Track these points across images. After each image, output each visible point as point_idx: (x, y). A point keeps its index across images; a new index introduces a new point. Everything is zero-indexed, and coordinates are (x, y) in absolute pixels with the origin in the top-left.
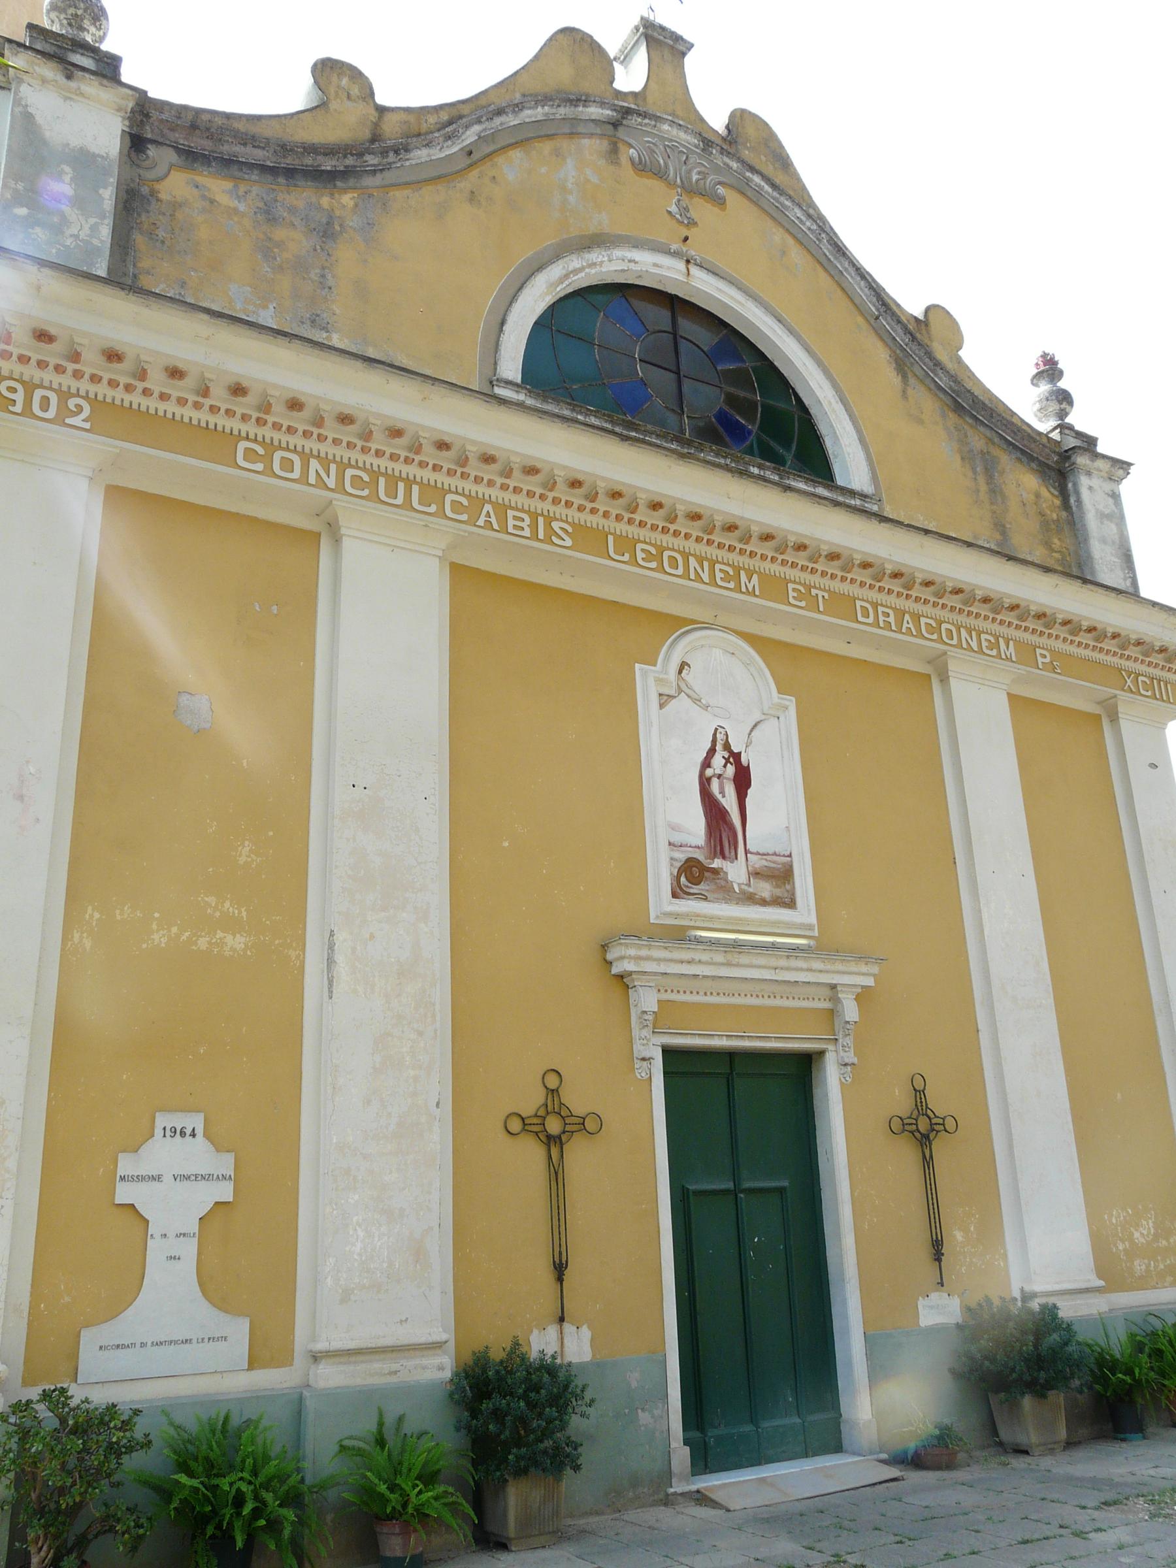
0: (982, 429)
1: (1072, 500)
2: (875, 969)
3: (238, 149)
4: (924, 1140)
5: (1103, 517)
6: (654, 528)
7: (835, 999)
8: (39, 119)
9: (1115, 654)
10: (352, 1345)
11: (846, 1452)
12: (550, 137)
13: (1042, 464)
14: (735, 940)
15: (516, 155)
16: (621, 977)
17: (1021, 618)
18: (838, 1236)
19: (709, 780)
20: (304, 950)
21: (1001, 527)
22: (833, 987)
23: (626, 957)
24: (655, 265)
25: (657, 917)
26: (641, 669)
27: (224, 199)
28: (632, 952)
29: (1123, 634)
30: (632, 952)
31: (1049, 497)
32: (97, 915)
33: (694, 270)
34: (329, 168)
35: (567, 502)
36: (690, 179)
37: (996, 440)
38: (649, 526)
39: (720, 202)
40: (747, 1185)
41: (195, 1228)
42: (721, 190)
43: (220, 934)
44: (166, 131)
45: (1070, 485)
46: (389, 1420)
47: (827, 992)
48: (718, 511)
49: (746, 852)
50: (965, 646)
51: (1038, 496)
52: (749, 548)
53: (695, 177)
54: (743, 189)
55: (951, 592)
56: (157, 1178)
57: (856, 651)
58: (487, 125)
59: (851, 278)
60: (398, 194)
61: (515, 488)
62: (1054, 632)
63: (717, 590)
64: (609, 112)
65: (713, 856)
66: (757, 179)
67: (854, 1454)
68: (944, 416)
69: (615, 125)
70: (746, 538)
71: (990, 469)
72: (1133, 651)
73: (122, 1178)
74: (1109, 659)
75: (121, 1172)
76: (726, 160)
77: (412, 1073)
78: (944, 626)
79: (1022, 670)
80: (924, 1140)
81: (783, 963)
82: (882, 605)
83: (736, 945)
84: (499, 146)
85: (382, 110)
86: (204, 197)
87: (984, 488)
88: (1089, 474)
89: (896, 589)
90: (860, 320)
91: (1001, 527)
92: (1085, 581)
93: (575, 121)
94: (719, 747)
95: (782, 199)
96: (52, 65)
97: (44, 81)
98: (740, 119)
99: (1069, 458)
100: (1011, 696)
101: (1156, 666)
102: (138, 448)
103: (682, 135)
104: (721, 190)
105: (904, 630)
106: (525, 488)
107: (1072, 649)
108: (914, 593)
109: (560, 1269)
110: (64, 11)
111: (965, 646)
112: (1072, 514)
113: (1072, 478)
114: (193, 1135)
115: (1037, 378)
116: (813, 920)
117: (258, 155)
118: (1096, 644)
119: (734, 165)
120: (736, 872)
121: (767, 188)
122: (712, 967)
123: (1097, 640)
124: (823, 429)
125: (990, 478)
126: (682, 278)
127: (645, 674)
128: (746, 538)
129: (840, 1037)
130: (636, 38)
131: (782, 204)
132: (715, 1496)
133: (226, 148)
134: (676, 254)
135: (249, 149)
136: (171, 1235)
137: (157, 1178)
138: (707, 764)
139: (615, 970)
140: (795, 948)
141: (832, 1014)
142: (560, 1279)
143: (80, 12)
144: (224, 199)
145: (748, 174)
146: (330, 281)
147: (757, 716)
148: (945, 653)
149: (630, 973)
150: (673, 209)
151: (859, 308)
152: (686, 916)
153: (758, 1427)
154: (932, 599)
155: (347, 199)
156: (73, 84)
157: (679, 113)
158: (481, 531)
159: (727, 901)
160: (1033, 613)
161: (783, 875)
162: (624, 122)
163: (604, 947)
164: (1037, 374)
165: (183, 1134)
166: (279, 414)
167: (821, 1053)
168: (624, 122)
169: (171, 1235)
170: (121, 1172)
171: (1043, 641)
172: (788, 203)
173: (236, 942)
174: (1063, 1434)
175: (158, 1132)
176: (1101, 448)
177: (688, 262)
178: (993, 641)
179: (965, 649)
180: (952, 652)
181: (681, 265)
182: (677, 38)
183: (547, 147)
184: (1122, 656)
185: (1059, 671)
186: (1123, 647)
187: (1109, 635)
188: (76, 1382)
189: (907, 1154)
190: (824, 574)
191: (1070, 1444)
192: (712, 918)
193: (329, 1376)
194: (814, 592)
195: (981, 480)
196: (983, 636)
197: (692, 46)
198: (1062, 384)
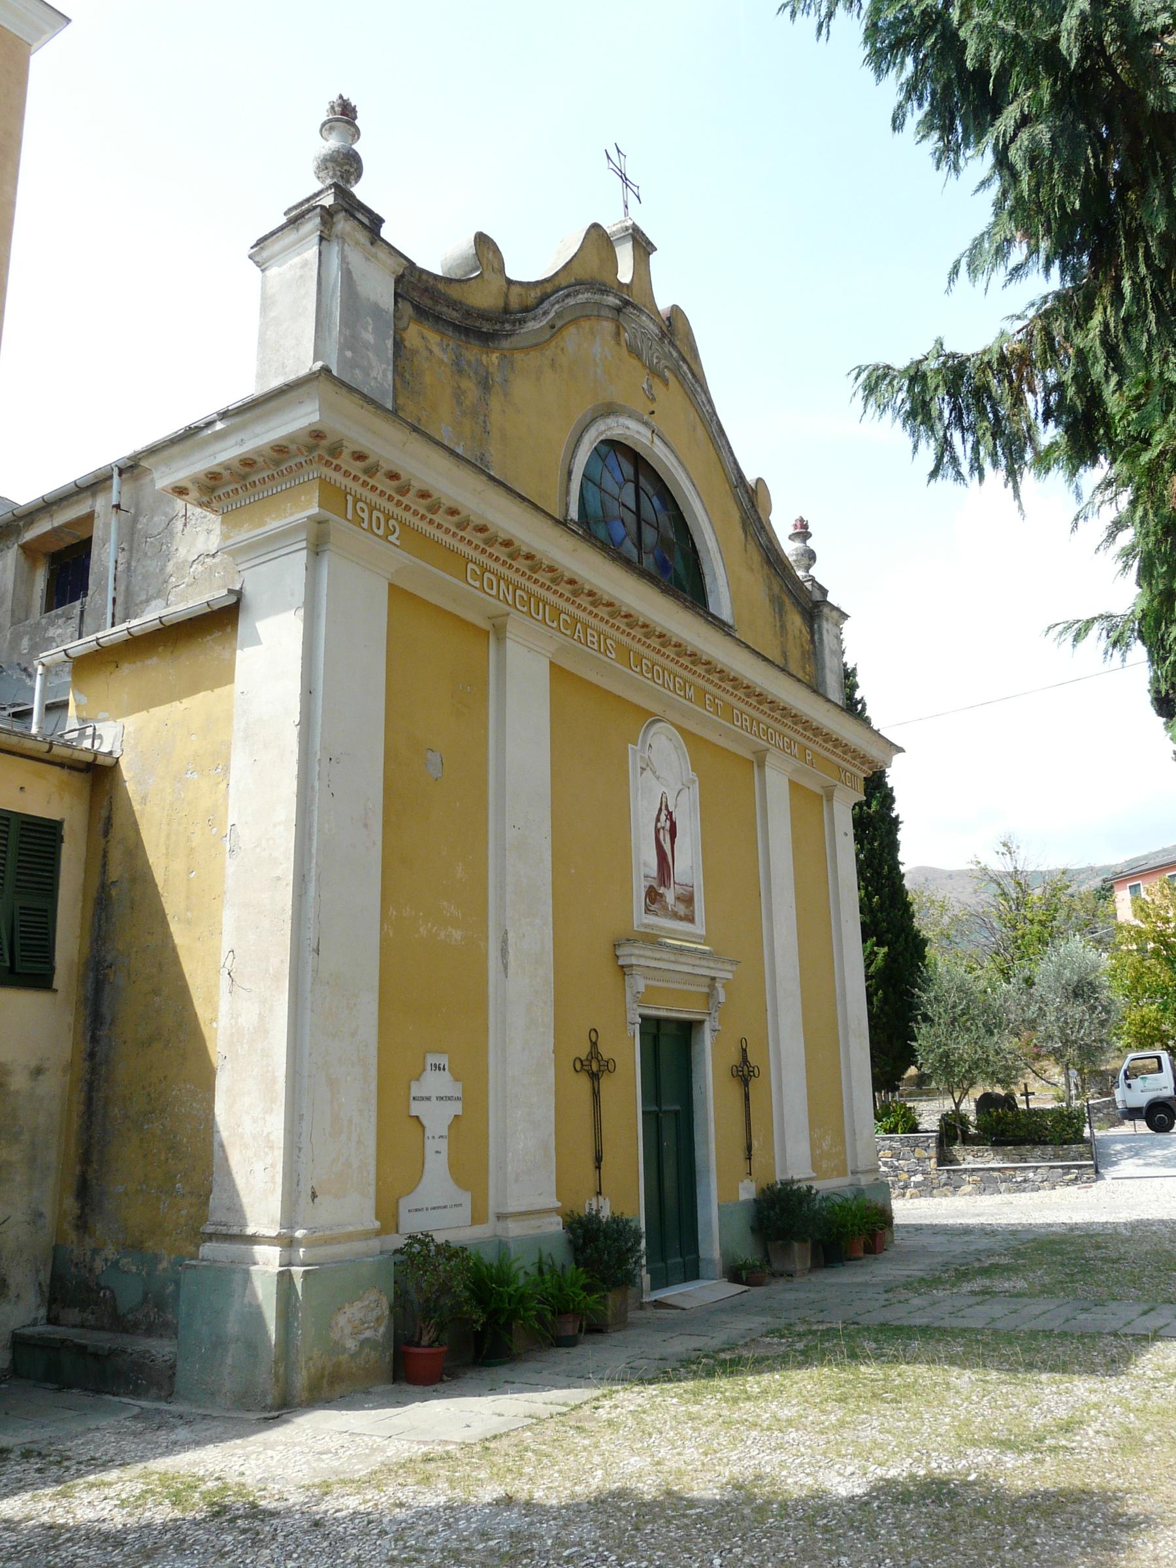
0: (778, 578)
1: (816, 637)
2: (734, 968)
3: (445, 309)
4: (594, 1077)
5: (833, 652)
6: (416, 513)
7: (712, 987)
8: (355, 277)
9: (523, 574)
10: (523, 1209)
11: (703, 1279)
12: (588, 317)
13: (804, 608)
14: (681, 946)
15: (572, 330)
16: (622, 967)
17: (612, 615)
18: (706, 1142)
19: (659, 830)
20: (487, 942)
21: (784, 655)
22: (713, 979)
23: (634, 955)
24: (638, 432)
25: (638, 927)
26: (632, 749)
27: (437, 350)
28: (637, 952)
29: (517, 543)
30: (637, 952)
31: (805, 630)
32: (395, 913)
33: (656, 439)
34: (485, 330)
35: (438, 524)
36: (652, 361)
37: (784, 588)
38: (444, 528)
39: (666, 382)
40: (664, 1108)
41: (446, 1133)
42: (667, 373)
43: (450, 929)
44: (410, 289)
45: (816, 626)
46: (544, 1255)
47: (708, 981)
48: (690, 644)
49: (675, 883)
50: (501, 597)
51: (801, 631)
52: (371, 482)
53: (655, 361)
54: (677, 373)
55: (501, 544)
56: (428, 1099)
57: (723, 742)
58: (561, 304)
59: (725, 454)
60: (518, 356)
61: (406, 506)
62: (578, 601)
63: (483, 595)
64: (617, 302)
65: (660, 886)
66: (685, 367)
67: (709, 1279)
68: (763, 568)
69: (618, 310)
70: (404, 490)
71: (781, 612)
72: (498, 551)
73: (414, 1098)
74: (439, 534)
75: (413, 1095)
76: (671, 349)
77: (542, 1030)
78: (487, 575)
79: (799, 764)
80: (594, 1077)
81: (697, 962)
82: (591, 628)
83: (681, 949)
84: (566, 320)
85: (510, 282)
86: (426, 346)
87: (778, 624)
88: (827, 620)
89: (475, 542)
90: (727, 485)
91: (784, 655)
92: (815, 691)
93: (599, 305)
94: (663, 807)
95: (696, 385)
96: (365, 233)
97: (357, 243)
98: (676, 310)
99: (819, 606)
100: (790, 781)
101: (497, 559)
102: (448, 577)
103: (651, 326)
104: (667, 373)
105: (576, 637)
106: (414, 507)
107: (424, 526)
108: (405, 501)
109: (598, 1159)
110: (341, 165)
111: (501, 597)
112: (815, 647)
113: (817, 621)
114: (444, 1069)
115: (327, 127)
116: (704, 932)
117: (455, 315)
118: (551, 585)
119: (675, 354)
120: (670, 896)
121: (690, 376)
122: (667, 963)
123: (553, 580)
124: (706, 569)
125: (781, 616)
126: (648, 444)
127: (634, 752)
128: (434, 508)
129: (713, 1012)
130: (623, 234)
131: (696, 390)
132: (669, 1302)
133: (438, 308)
134: (646, 424)
135: (450, 311)
136: (436, 1137)
137: (428, 1099)
138: (658, 820)
139: (621, 962)
140: (704, 953)
141: (710, 995)
142: (598, 1167)
143: (352, 170)
144: (437, 350)
145: (681, 363)
146: (488, 428)
147: (681, 787)
148: (768, 750)
149: (631, 966)
150: (645, 386)
151: (728, 480)
152: (662, 928)
153: (666, 1263)
154: (453, 529)
155: (494, 357)
156: (373, 250)
157: (648, 305)
158: (737, 729)
159: (666, 916)
160: (500, 540)
161: (687, 900)
162: (624, 310)
163: (616, 946)
164: (793, 534)
165: (440, 1069)
166: (345, 461)
167: (701, 1022)
168: (624, 310)
169: (436, 1137)
170: (413, 1095)
171: (810, 744)
172: (699, 389)
173: (457, 935)
174: (809, 1264)
175: (429, 1067)
176: (385, 233)
177: (653, 432)
178: (526, 599)
179: (349, 520)
180: (774, 750)
181: (649, 434)
182: (649, 243)
183: (586, 325)
184: (530, 578)
185: (613, 656)
186: (576, 593)
187: (640, 623)
188: (397, 1232)
189: (583, 1084)
190: (439, 526)
191: (810, 1271)
192: (675, 931)
193: (515, 1229)
194: (717, 701)
195: (777, 616)
196: (519, 592)
197: (656, 249)
198: (809, 542)
